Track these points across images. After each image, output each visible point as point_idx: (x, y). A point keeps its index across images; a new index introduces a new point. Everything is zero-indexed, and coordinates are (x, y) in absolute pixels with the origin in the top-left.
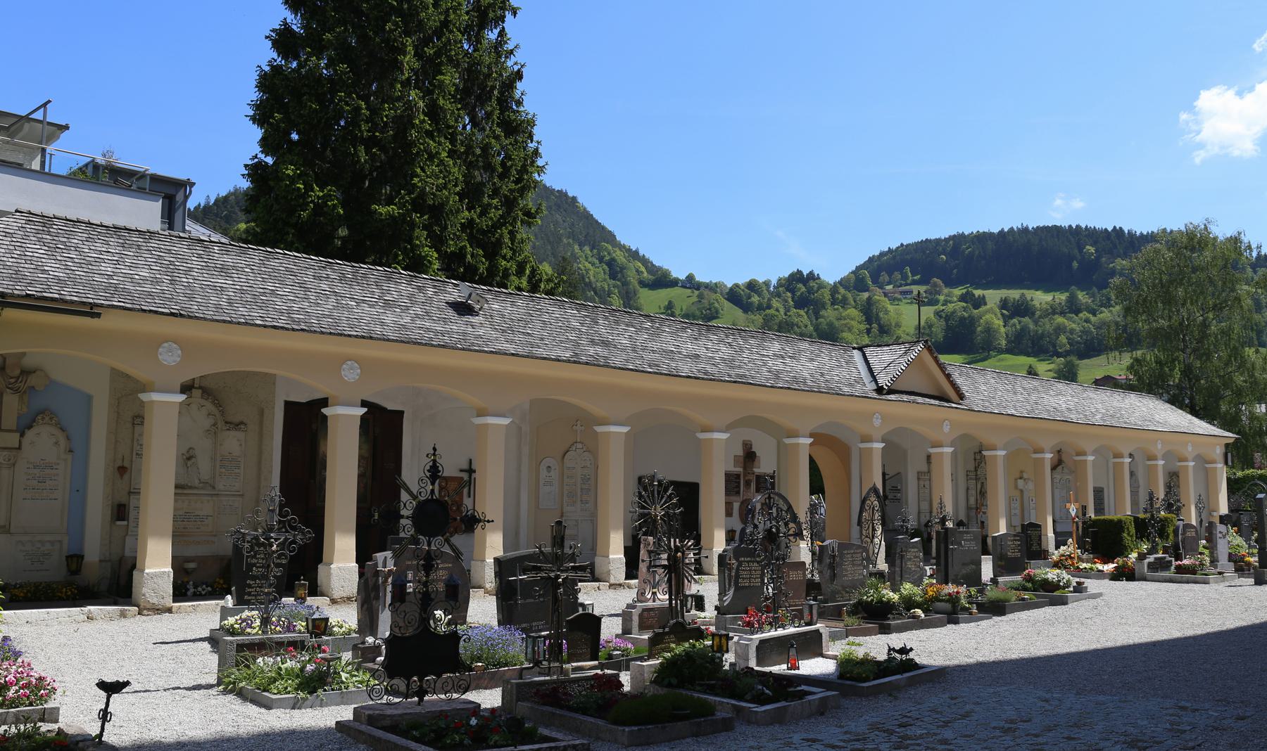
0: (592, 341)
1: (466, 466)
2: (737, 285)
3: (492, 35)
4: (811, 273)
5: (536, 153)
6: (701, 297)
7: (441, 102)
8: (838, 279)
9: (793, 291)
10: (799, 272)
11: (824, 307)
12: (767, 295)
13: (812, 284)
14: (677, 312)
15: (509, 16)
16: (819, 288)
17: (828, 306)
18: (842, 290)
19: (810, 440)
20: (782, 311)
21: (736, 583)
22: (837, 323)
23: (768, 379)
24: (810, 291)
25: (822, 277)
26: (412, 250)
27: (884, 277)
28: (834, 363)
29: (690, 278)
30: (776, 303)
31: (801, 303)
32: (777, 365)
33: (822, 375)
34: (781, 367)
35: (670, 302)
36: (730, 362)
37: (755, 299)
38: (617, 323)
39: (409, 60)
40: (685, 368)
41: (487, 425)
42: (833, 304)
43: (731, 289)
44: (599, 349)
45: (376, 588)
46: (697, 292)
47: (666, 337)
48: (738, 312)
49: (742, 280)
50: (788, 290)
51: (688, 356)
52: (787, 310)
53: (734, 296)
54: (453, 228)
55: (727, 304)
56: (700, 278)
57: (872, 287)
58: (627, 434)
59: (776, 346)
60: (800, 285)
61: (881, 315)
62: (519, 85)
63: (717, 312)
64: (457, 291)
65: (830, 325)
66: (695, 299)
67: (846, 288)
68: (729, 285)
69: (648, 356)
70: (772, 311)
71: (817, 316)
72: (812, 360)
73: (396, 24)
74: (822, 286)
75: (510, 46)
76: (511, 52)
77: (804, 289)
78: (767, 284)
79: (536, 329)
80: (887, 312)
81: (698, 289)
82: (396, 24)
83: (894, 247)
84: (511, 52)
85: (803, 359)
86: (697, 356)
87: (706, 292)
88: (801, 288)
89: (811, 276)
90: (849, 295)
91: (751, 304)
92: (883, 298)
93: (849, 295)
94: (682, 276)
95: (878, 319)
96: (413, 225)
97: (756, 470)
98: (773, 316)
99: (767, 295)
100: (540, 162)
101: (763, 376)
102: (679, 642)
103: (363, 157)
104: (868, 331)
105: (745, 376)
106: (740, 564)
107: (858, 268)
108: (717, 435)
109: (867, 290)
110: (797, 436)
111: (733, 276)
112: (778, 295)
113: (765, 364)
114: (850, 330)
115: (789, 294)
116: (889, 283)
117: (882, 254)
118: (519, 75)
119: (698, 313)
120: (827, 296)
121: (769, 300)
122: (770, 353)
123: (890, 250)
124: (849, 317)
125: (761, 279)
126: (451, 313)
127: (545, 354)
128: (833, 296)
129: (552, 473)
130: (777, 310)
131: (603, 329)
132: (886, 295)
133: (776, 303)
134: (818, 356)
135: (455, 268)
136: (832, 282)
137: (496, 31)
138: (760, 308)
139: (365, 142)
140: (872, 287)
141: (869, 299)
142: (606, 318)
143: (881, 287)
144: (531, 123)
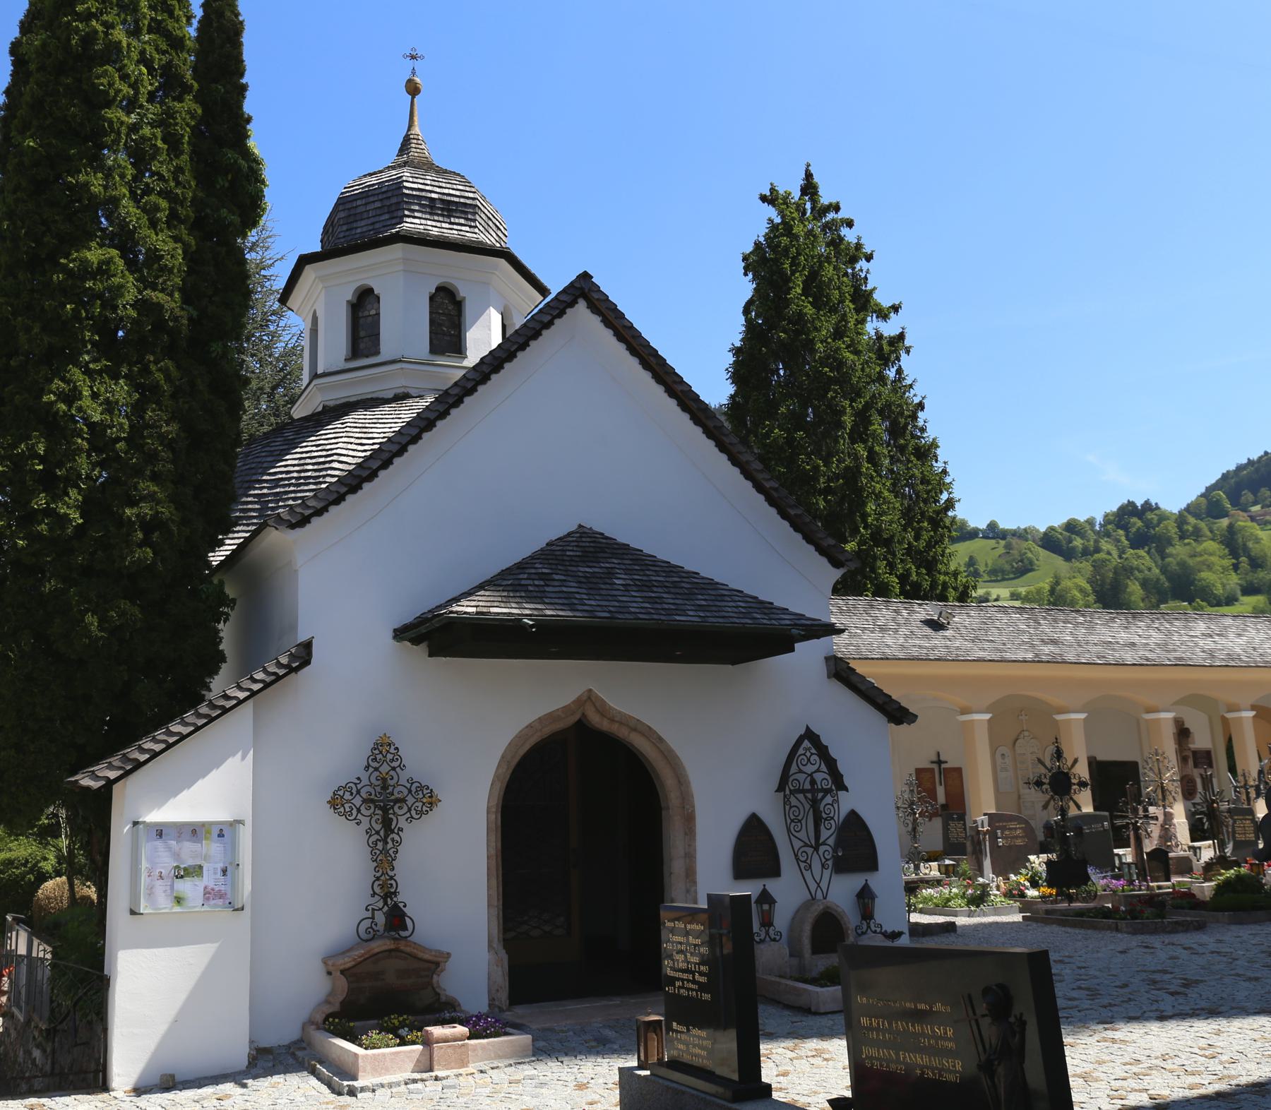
0: (1043, 641)
1: (935, 759)
2: (1052, 529)
3: (891, 373)
4: (1147, 503)
5: (945, 472)
6: (1008, 547)
7: (877, 448)
8: (1183, 506)
9: (1125, 528)
10: (1131, 504)
11: (1169, 542)
12: (1092, 537)
13: (1149, 516)
14: (982, 569)
15: (903, 355)
16: (1160, 522)
17: (1176, 541)
18: (1192, 520)
19: (1252, 714)
20: (1115, 553)
21: (1234, 837)
22: (1191, 562)
23: (1205, 659)
24: (1148, 524)
25: (1161, 506)
26: (876, 578)
27: (1247, 496)
28: (1262, 635)
29: (992, 526)
30: (1105, 545)
31: (1139, 541)
32: (1208, 644)
33: (1254, 649)
34: (1213, 646)
35: (971, 558)
36: (1164, 646)
37: (1078, 542)
38: (1055, 621)
39: (848, 420)
40: (1129, 657)
41: (1158, 720)
42: (1182, 538)
43: (1045, 534)
44: (1052, 648)
45: (979, 843)
46: (1003, 543)
47: (1100, 629)
48: (1058, 561)
49: (1058, 521)
50: (1119, 526)
51: (1125, 645)
52: (1122, 552)
53: (1049, 541)
54: (900, 550)
55: (1043, 553)
56: (1005, 524)
57: (1233, 512)
58: (989, 721)
59: (1201, 627)
60: (1134, 520)
61: (1250, 544)
62: (920, 414)
63: (1031, 563)
64: (928, 610)
65: (1182, 564)
66: (1001, 550)
67: (1197, 516)
68: (1043, 529)
69: (1095, 649)
70: (1102, 556)
71: (1163, 556)
72: (1240, 635)
73: (835, 391)
74: (1163, 517)
75: (908, 382)
76: (911, 386)
77: (1139, 524)
78: (1091, 522)
79: (993, 634)
80: (1258, 540)
81: (1004, 538)
82: (835, 391)
83: (1255, 457)
84: (911, 386)
85: (1231, 636)
86: (1133, 644)
87: (1014, 541)
88: (1136, 522)
89: (1147, 506)
90: (1202, 525)
91: (1074, 548)
92: (1249, 524)
93: (1202, 525)
94: (982, 525)
95: (1246, 551)
96: (875, 558)
97: (1191, 746)
98: (1104, 561)
99: (1092, 537)
100: (948, 480)
101: (1199, 657)
102: (1227, 869)
103: (822, 504)
104: (1236, 567)
105: (1181, 659)
106: (1235, 822)
107: (1210, 489)
108: (1163, 715)
109: (1226, 515)
110: (1239, 710)
111: (1046, 519)
112: (1108, 535)
113: (1196, 645)
114: (1210, 567)
115: (1121, 532)
116: (1255, 503)
117: (1240, 468)
118: (921, 406)
119: (1007, 567)
120: (1173, 531)
121: (1096, 541)
122: (1198, 633)
123: (1250, 462)
124: (1205, 552)
125: (1082, 518)
126: (928, 631)
127: (1013, 657)
128: (1180, 527)
129: (1007, 760)
130: (1109, 553)
131: (1046, 627)
132: (1253, 519)
133: (1105, 545)
134: (1244, 630)
135: (913, 592)
136: (1176, 511)
137: (894, 370)
138: (1086, 552)
139: (821, 492)
140: (1233, 512)
141: (1231, 526)
142: (1045, 618)
143: (1245, 510)
144: (934, 445)
